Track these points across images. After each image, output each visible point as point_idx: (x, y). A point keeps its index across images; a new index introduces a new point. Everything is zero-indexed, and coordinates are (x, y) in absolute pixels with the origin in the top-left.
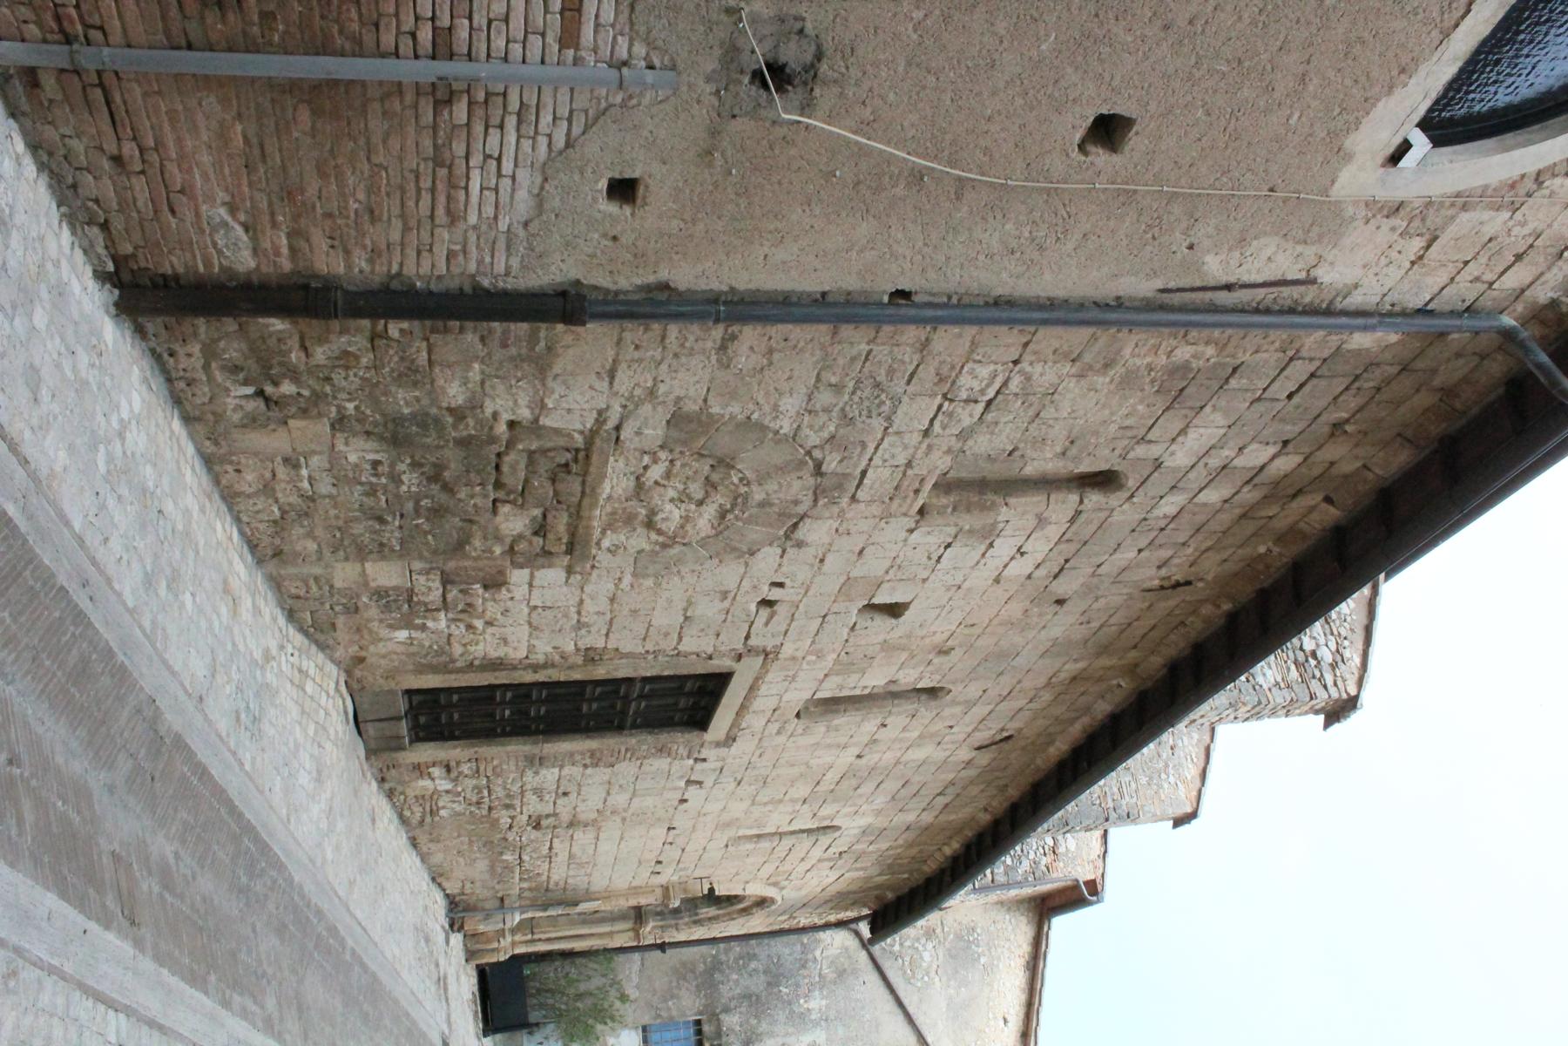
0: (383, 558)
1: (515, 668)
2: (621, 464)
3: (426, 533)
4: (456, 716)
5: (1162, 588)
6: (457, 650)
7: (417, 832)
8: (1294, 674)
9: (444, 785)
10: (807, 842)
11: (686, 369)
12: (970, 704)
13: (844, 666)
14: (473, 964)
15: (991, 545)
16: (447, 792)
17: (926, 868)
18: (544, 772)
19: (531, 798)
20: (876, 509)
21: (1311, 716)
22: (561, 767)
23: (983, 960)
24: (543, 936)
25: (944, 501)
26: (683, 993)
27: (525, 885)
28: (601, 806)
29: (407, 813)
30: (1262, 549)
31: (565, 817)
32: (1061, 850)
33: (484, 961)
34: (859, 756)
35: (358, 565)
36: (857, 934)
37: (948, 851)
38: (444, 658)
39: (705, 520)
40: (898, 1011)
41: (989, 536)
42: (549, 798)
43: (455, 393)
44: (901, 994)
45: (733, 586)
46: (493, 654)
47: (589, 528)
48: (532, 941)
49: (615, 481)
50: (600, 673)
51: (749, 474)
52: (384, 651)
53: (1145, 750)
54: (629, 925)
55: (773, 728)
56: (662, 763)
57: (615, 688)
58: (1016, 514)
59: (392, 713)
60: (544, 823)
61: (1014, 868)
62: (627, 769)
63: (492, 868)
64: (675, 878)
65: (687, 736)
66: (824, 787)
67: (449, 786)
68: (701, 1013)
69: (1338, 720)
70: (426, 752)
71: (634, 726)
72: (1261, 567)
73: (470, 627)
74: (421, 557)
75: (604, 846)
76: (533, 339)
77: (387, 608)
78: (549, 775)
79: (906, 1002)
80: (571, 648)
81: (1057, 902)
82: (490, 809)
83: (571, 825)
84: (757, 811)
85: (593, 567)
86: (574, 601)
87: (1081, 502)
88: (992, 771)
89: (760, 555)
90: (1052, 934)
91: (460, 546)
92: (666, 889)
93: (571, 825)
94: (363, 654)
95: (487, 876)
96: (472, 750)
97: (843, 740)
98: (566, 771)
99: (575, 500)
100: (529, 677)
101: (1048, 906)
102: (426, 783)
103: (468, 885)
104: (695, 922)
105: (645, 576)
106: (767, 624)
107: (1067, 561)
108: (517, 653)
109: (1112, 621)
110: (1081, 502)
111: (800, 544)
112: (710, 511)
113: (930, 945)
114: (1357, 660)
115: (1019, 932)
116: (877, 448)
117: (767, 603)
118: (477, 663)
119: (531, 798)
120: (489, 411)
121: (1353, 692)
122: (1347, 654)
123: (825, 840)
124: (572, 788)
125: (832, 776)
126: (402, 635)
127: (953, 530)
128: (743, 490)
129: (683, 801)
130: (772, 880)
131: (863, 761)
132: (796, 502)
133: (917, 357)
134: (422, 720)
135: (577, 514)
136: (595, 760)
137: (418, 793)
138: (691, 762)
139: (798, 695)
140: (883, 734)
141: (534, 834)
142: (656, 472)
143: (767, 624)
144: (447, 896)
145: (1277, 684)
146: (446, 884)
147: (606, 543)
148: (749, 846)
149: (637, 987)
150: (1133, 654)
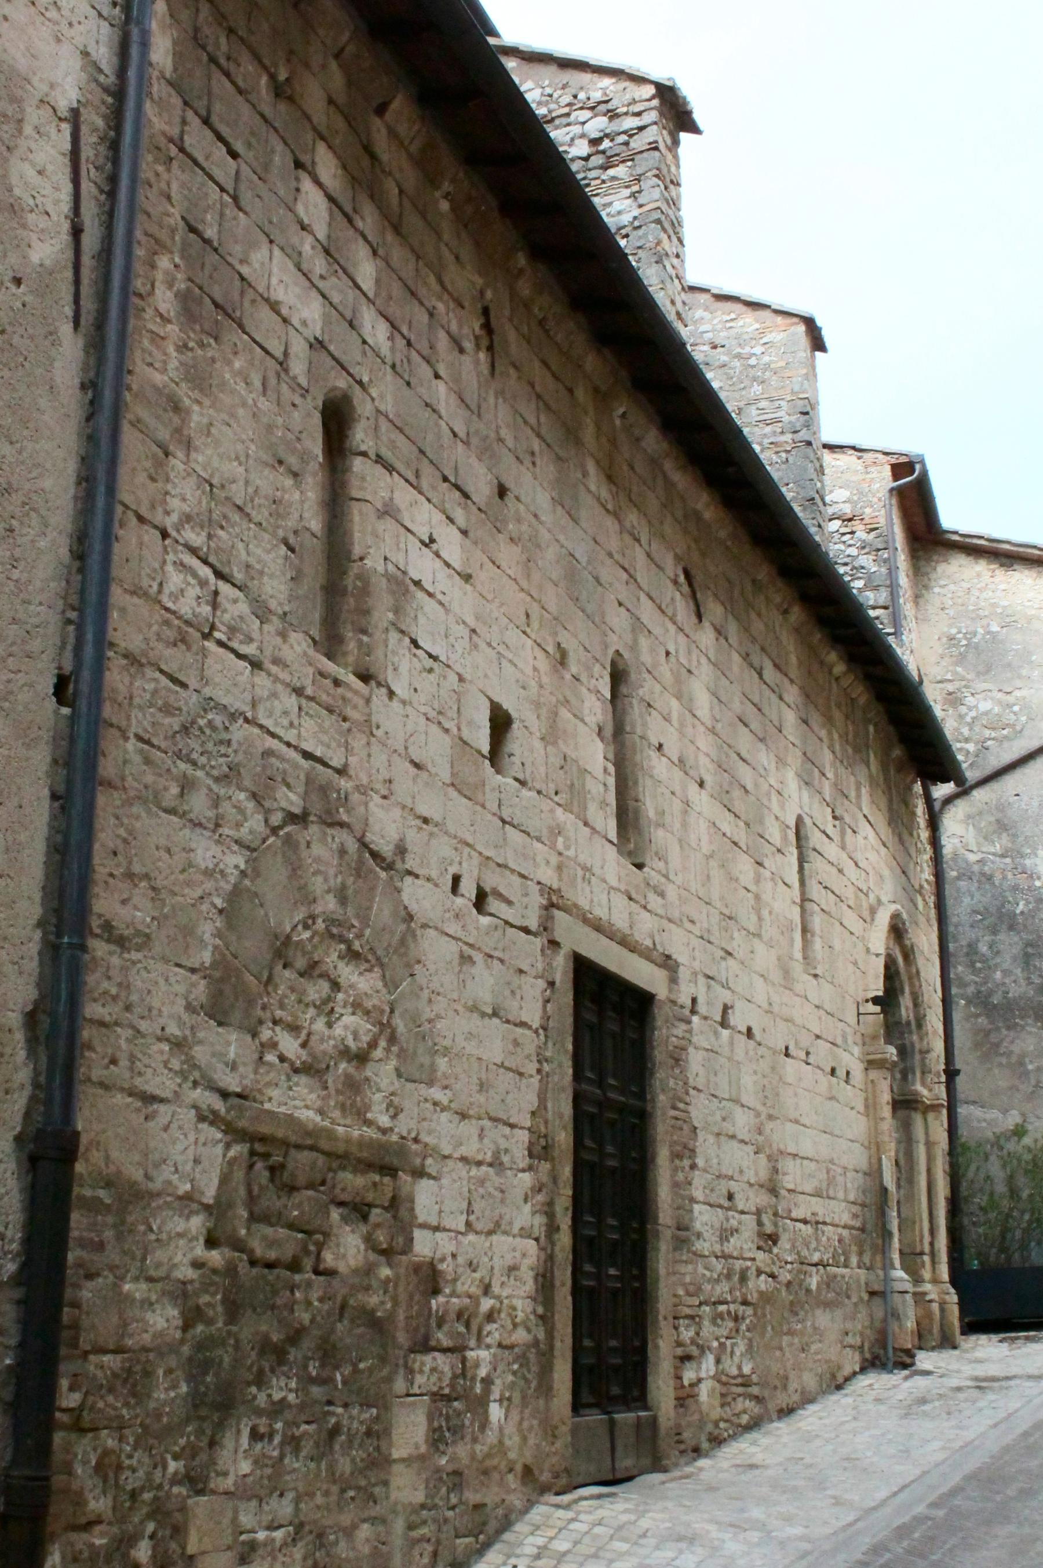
0: (387, 1432)
1: (551, 1258)
2: (275, 1093)
5: (490, 348)
6: (521, 1336)
8: (620, 171)
9: (708, 1365)
10: (816, 865)
11: (149, 995)
12: (638, 625)
13: (574, 798)
15: (417, 583)
16: (718, 1361)
18: (698, 1226)
19: (733, 1245)
21: (681, 151)
23: (995, 628)
24: (927, 1239)
25: (352, 646)
27: (854, 1260)
28: (750, 1149)
29: (745, 1419)
30: (445, 206)
33: (956, 1323)
34: (701, 784)
36: (949, 800)
37: (840, 668)
38: (532, 1356)
41: (404, 586)
43: (162, 1319)
45: (454, 947)
47: (361, 1143)
48: (933, 1254)
50: (564, 1138)
52: (517, 1439)
53: (715, 385)
54: (918, 1119)
56: (695, 1060)
57: (585, 1119)
60: (769, 1229)
62: (700, 1109)
63: (827, 1305)
64: (856, 1051)
65: (659, 1023)
67: (711, 1358)
69: (688, 114)
70: (662, 1390)
72: (469, 209)
73: (490, 1317)
74: (389, 1380)
78: (703, 1218)
80: (527, 1178)
81: (919, 520)
82: (745, 1303)
83: (773, 1191)
84: (770, 931)
85: (416, 1140)
86: (461, 1169)
87: (364, 454)
90: (964, 529)
91: (377, 1325)
92: (871, 1064)
93: (773, 1191)
95: (839, 1313)
96: (662, 1323)
100: (565, 1239)
102: (704, 1391)
103: (850, 1340)
104: (919, 1026)
106: (509, 903)
107: (445, 479)
109: (533, 421)
110: (364, 454)
111: (401, 850)
113: (970, 700)
117: (480, 901)
118: (540, 1310)
119: (733, 1245)
120: (190, 1273)
123: (815, 839)
124: (723, 1187)
125: (727, 823)
127: (394, 636)
128: (320, 925)
130: (866, 914)
131: (708, 779)
132: (342, 852)
134: (615, 1390)
136: (685, 1152)
138: (695, 1019)
140: (672, 749)
141: (784, 1243)
142: (289, 1045)
143: (509, 903)
145: (633, 195)
146: (847, 1371)
147: (384, 1120)
148: (818, 944)
150: (580, 394)
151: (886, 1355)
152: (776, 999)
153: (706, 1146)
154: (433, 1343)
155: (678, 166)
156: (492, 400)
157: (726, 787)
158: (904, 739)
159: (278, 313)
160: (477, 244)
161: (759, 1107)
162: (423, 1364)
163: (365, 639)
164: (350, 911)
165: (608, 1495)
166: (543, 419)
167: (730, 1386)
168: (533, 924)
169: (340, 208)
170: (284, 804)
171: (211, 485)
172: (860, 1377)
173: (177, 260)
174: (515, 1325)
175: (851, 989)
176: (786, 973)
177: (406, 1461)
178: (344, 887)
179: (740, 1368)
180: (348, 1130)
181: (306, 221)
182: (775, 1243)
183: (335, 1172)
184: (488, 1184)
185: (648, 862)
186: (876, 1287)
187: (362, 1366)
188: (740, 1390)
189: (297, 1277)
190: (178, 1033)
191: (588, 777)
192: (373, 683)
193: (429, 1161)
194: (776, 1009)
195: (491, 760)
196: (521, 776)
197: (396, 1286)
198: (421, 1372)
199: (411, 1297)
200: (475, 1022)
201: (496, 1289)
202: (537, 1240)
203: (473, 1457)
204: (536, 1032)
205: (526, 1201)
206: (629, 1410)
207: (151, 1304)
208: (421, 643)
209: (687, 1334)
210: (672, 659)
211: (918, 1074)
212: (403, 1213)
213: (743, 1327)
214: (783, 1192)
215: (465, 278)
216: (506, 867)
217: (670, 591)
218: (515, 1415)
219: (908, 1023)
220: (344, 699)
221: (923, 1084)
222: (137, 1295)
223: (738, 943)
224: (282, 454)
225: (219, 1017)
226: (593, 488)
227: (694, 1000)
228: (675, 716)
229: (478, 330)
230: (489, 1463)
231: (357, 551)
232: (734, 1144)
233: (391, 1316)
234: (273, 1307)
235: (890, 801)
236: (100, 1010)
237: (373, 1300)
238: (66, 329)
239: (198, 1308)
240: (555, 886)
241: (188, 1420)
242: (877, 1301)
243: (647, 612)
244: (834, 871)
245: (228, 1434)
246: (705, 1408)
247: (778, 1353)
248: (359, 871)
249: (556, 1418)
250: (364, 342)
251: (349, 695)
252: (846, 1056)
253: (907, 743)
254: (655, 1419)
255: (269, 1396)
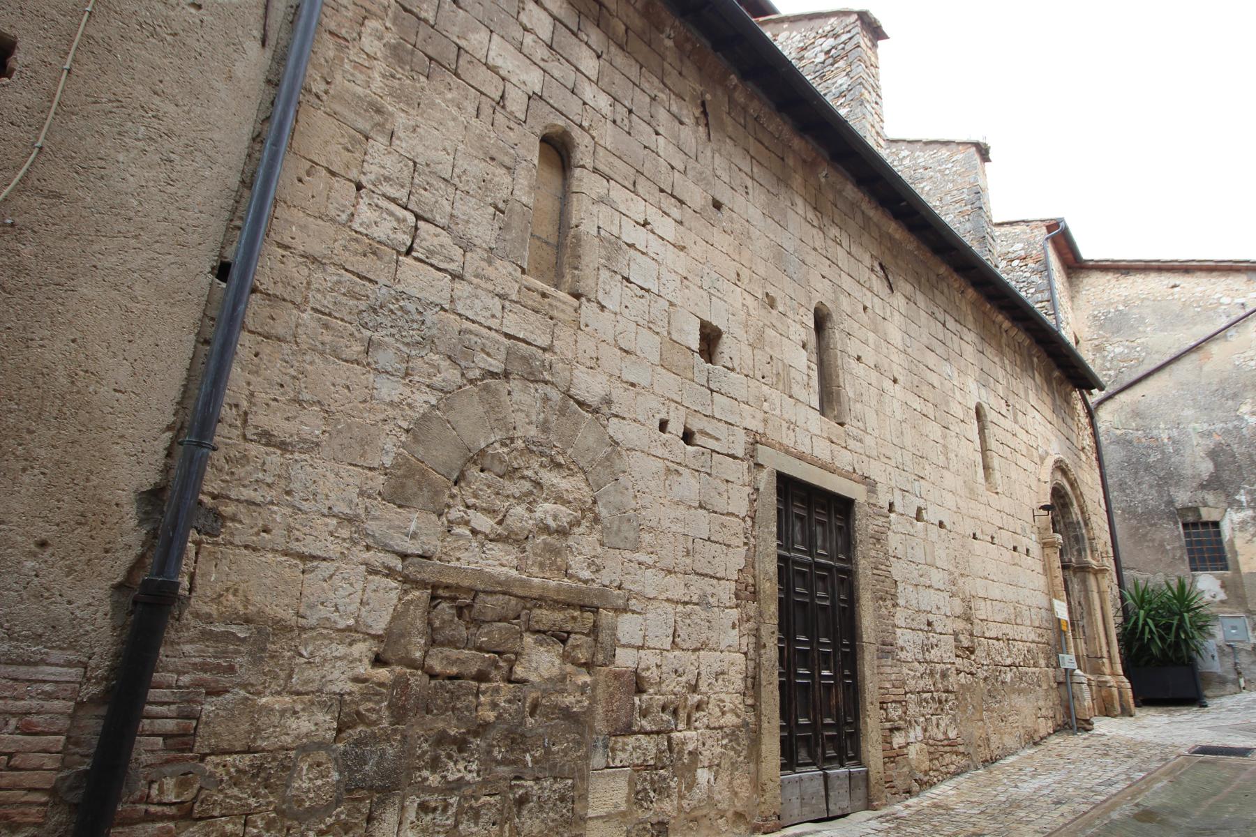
0: (584, 797)
1: (758, 666)
2: (464, 555)
3: (548, 752)
4: (828, 721)
5: (707, 125)
6: (730, 720)
7: (978, 758)
8: (841, 64)
9: (916, 733)
10: (991, 430)
12: (837, 287)
13: (782, 380)
14: (1137, 711)
15: (631, 246)
16: (925, 730)
17: (1027, 342)
18: (900, 642)
19: (934, 654)
20: (565, 333)
21: (879, 51)
22: (895, 626)
23: (1121, 308)
24: (1105, 649)
25: (568, 278)
26: (1158, 536)
27: (1042, 662)
28: (946, 595)
29: (952, 768)
30: (669, 43)
31: (960, 625)
32: (1023, 253)
33: (1131, 701)
34: (895, 381)
35: (591, 824)
36: (1101, 403)
37: (1007, 324)
38: (742, 735)
40: (1167, 370)
41: (614, 246)
43: (312, 723)
44: (1153, 367)
45: (660, 464)
46: (739, 684)
47: (558, 590)
48: (1110, 658)
50: (770, 587)
51: (499, 435)
52: (727, 794)
53: (842, 112)
54: (1092, 580)
55: (852, 444)
56: (894, 541)
58: (589, 218)
59: (818, 785)
60: (966, 643)
61: (1038, 286)
63: (1020, 692)
64: (1034, 537)
65: (858, 517)
66: (930, 410)
67: (919, 729)
68: (1176, 523)
69: (879, 27)
70: (873, 751)
71: (849, 560)
72: (688, 46)
73: (698, 707)
74: (587, 757)
75: (995, 593)
77: (662, 791)
78: (903, 637)
79: (1159, 363)
80: (735, 614)
81: (1070, 256)
82: (947, 691)
83: (968, 620)
84: (954, 465)
85: (619, 588)
86: (669, 607)
87: (583, 166)
88: (919, 283)
89: (618, 437)
90: (1096, 258)
92: (1045, 545)
93: (968, 620)
94: (729, 814)
95: (1032, 697)
96: (869, 707)
97: (873, 391)
98: (901, 622)
99: (513, 601)
100: (771, 653)
101: (1074, 265)
102: (912, 752)
103: (1044, 712)
104: (1086, 525)
105: (638, 539)
106: (717, 439)
107: (662, 191)
108: (737, 664)
109: (748, 170)
110: (583, 166)
111: (608, 401)
112: (550, 478)
113: (1109, 348)
114: (833, 20)
115: (1097, 287)
116: (473, 322)
117: (688, 437)
118: (750, 701)
119: (934, 654)
120: (350, 686)
121: (856, 17)
122: (828, 28)
123: (991, 416)
124: (923, 618)
125: (917, 404)
126: (703, 775)
127: (604, 274)
128: (520, 444)
129: (941, 524)
130: (1037, 460)
131: (901, 378)
132: (546, 399)
133: (331, 269)
134: (831, 753)
135: (540, 600)
136: (888, 596)
137: (925, 758)
138: (892, 515)
139: (815, 422)
140: (869, 357)
141: (980, 653)
142: (484, 523)
143: (717, 439)
144: (1055, 731)
145: (847, 74)
146: (1043, 733)
147: (586, 574)
148: (997, 475)
149: (1154, 574)
150: (791, 162)
151: (1071, 722)
152: (961, 504)
153: (905, 594)
154: (636, 728)
155: (877, 58)
156: (709, 154)
157: (915, 383)
158: (1060, 366)
159: (497, 74)
160: (700, 69)
161: (952, 569)
162: (625, 744)
163: (576, 272)
164: (552, 437)
166: (755, 170)
167: (935, 749)
168: (740, 454)
169: (561, 22)
170: (481, 365)
171: (415, 163)
172: (1053, 737)
173: (388, 25)
174: (723, 713)
175: (1027, 501)
176: (972, 490)
177: (607, 818)
178: (546, 421)
179: (945, 733)
180: (542, 581)
181: (529, 26)
182: (972, 653)
183: (530, 609)
184: (694, 617)
185: (848, 420)
186: (1061, 680)
187: (555, 749)
188: (948, 749)
189: (483, 686)
190: (347, 511)
191: (792, 370)
192: (583, 299)
193: (633, 602)
194: (964, 511)
195: (702, 353)
196: (730, 365)
197: (594, 689)
198: (623, 750)
199: (612, 696)
200: (681, 511)
201: (703, 687)
202: (745, 654)
203: (680, 809)
204: (743, 519)
205: (734, 627)
206: (842, 766)
207: (295, 712)
208: (632, 279)
209: (895, 713)
210: (869, 310)
211: (1088, 552)
212: (604, 636)
213: (947, 707)
214: (976, 621)
215: (692, 84)
216: (713, 417)
217: (865, 274)
218: (725, 777)
219: (1078, 523)
220: (550, 305)
221: (1093, 558)
222: (277, 706)
223: (928, 471)
224: (493, 152)
225: (398, 502)
226: (800, 212)
227: (891, 505)
228: (871, 341)
229: (697, 114)
230: (697, 813)
231: (574, 222)
232: (932, 591)
233: (590, 711)
234: (454, 709)
235: (1054, 400)
236: (253, 494)
237: (568, 700)
238: (253, 47)
239: (358, 713)
240: (761, 431)
241: (338, 802)
242: (1063, 688)
243: (847, 283)
244: (1009, 435)
245: (390, 810)
246: (914, 764)
247: (980, 723)
248: (562, 412)
249: (764, 777)
250: (585, 103)
251: (555, 303)
252: (1025, 541)
253: (1064, 370)
254: (867, 772)
255: (444, 777)
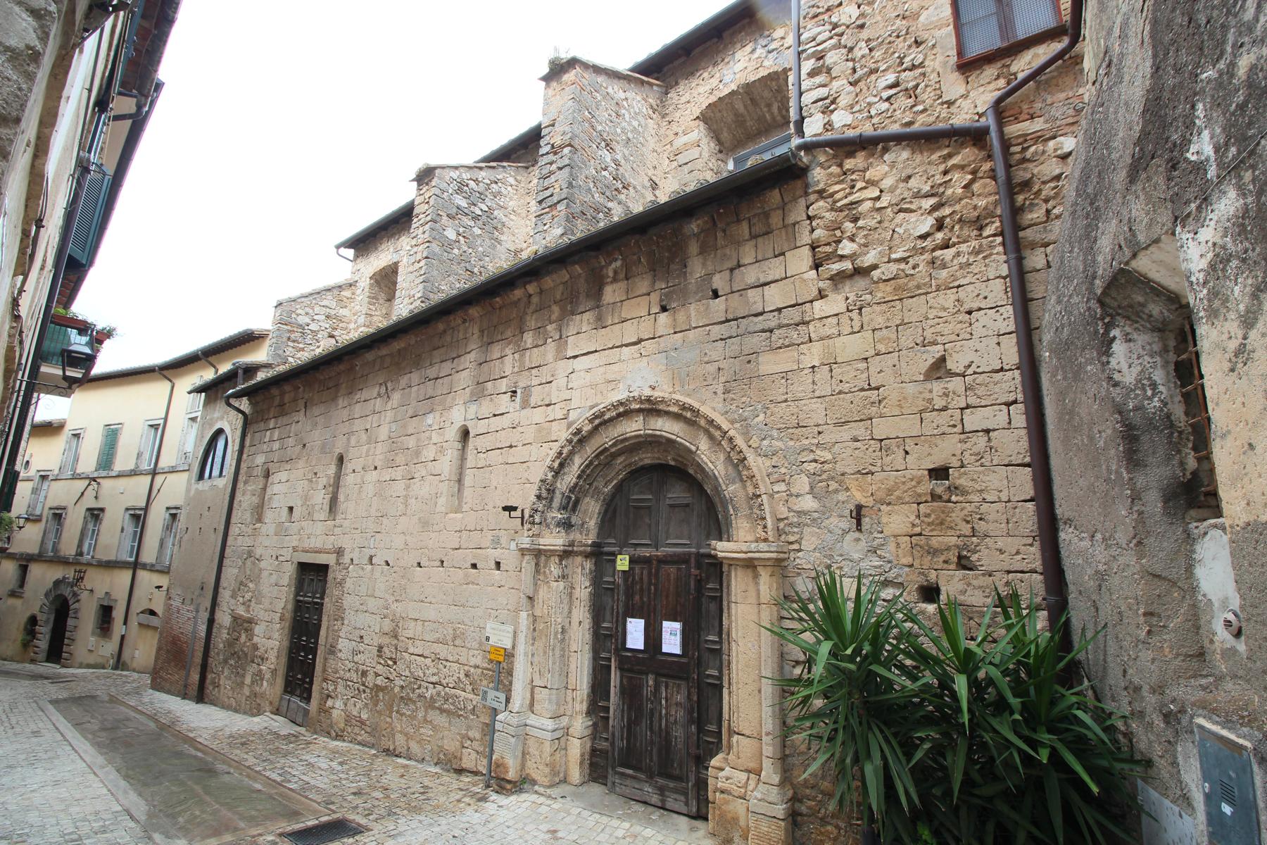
11: (225, 595)
28: (378, 617)
39: (251, 585)
42: (362, 647)
49: (241, 611)
56: (349, 584)
57: (299, 606)
62: (348, 601)
76: (1068, 522)
78: (343, 644)
83: (396, 637)
91: (246, 655)
124: (358, 633)
126: (265, 683)
153: (350, 617)
165: (28, 245)
